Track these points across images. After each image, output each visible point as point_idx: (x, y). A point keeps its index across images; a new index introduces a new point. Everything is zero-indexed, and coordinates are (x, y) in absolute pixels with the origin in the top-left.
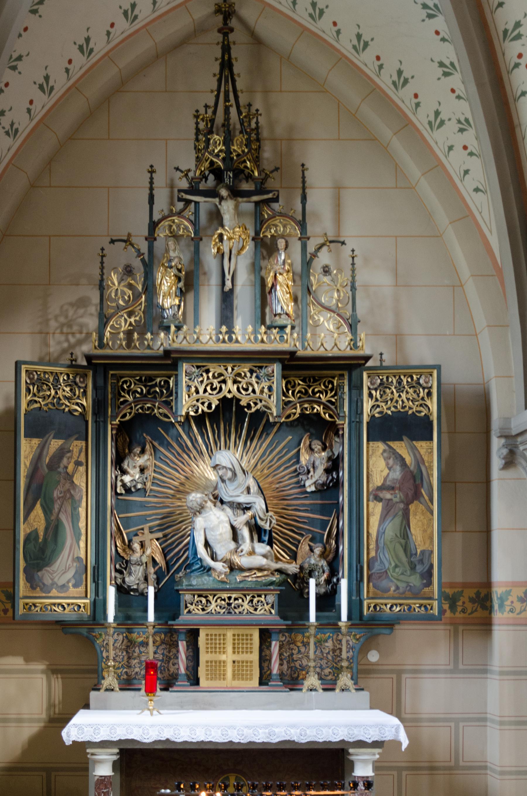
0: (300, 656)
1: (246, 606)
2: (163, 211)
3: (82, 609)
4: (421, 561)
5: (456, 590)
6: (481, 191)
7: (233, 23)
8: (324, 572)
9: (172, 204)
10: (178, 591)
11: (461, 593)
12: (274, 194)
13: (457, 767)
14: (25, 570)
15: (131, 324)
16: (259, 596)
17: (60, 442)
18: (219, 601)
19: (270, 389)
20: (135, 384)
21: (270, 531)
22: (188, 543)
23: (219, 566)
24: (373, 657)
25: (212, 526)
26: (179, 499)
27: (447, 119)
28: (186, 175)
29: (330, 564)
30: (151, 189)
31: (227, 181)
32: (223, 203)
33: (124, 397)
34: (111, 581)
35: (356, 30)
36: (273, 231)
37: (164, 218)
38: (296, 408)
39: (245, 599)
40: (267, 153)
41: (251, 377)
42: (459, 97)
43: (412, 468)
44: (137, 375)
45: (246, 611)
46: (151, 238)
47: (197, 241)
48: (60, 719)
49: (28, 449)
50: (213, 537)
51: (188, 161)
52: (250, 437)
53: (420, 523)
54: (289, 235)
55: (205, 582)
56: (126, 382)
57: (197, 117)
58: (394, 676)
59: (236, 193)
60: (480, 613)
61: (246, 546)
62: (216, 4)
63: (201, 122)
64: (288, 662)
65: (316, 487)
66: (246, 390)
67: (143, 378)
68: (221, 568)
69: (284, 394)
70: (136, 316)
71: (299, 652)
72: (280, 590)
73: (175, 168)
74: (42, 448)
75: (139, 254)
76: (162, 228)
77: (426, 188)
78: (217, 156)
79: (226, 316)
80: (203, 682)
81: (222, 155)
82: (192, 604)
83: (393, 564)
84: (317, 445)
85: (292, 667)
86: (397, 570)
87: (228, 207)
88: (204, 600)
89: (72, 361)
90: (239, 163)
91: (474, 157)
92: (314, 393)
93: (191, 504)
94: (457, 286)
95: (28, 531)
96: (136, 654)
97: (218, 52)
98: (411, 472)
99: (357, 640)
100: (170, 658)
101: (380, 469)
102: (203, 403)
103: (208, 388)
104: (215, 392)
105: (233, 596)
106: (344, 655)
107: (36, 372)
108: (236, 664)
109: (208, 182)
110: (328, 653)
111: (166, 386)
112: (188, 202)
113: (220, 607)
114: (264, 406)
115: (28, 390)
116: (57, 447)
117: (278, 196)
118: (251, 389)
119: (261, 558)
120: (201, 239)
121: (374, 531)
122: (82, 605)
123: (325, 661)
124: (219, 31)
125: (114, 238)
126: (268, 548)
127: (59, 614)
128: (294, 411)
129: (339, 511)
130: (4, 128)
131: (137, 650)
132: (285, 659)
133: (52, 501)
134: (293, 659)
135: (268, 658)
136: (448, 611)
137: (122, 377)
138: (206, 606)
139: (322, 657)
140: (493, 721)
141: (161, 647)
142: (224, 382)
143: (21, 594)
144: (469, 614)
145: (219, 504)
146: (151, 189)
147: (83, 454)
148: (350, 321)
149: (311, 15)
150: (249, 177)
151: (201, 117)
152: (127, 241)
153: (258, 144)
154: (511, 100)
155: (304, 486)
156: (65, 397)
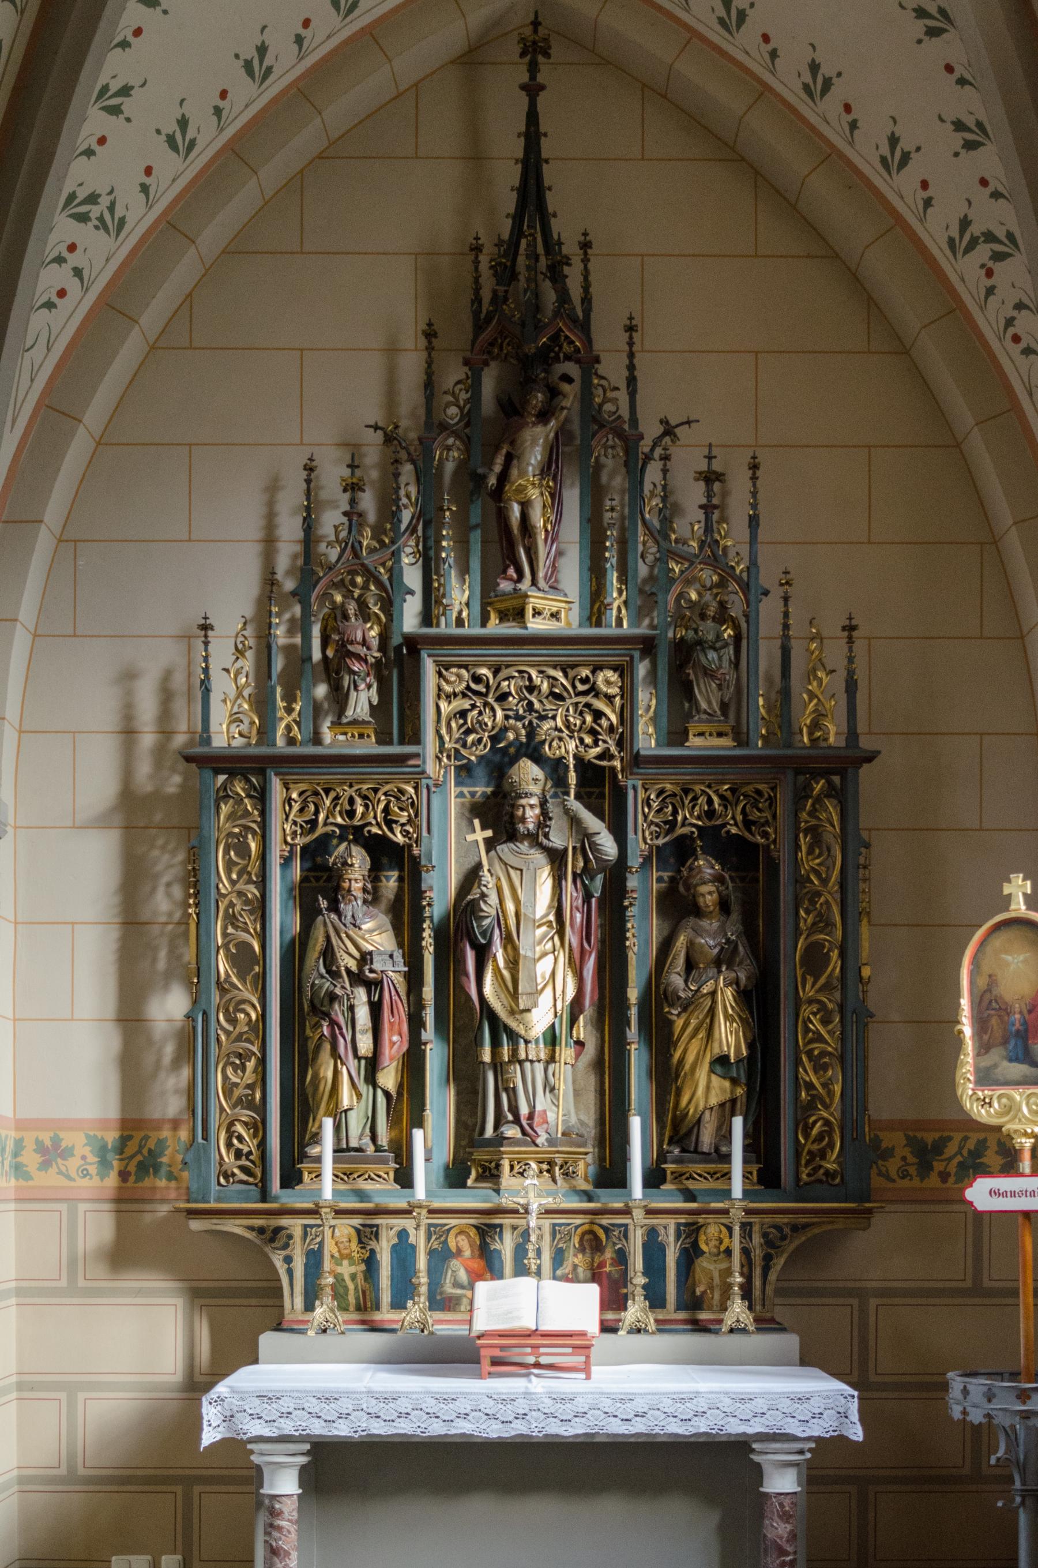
35: (808, 55)
48: (197, 1384)
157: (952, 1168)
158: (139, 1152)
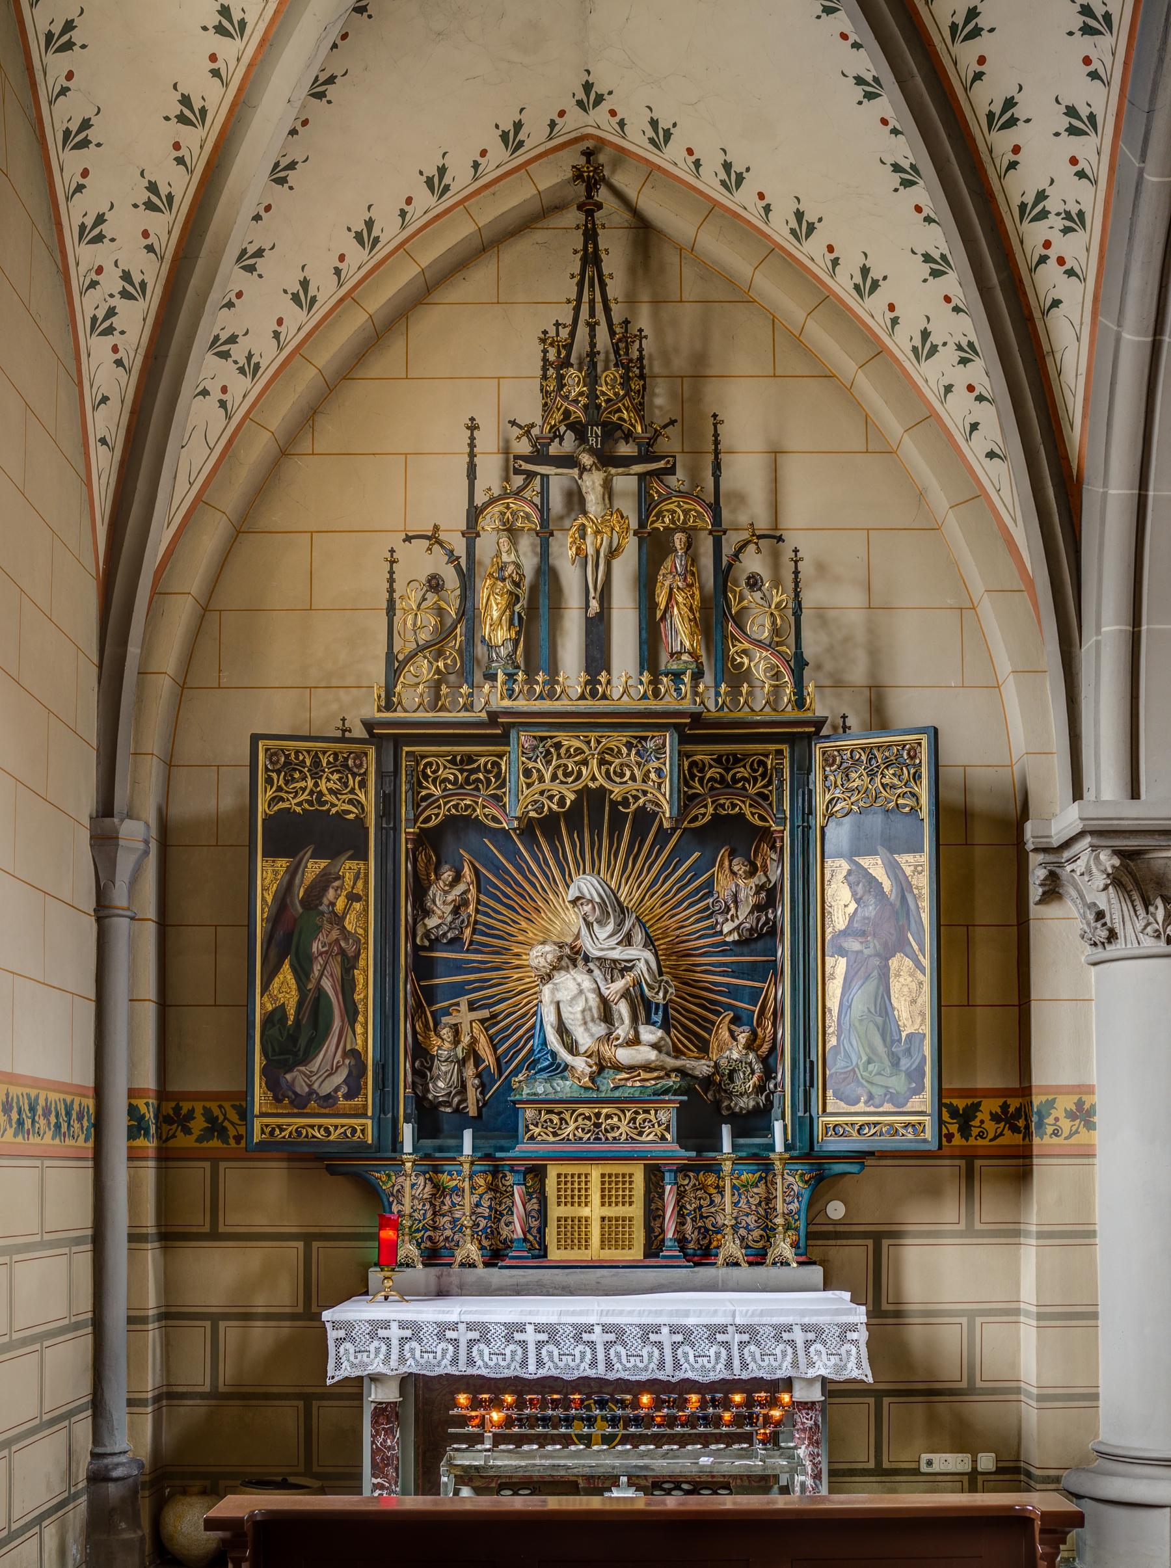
0: (713, 1210)
1: (624, 1128)
2: (490, 489)
3: (359, 1133)
4: (908, 1052)
5: (969, 1101)
6: (999, 456)
7: (602, 194)
8: (753, 1072)
9: (507, 479)
10: (514, 1102)
11: (976, 1107)
12: (668, 462)
13: (971, 1390)
14: (264, 1072)
15: (438, 671)
16: (647, 1112)
17: (323, 863)
18: (580, 1119)
19: (659, 771)
20: (445, 767)
21: (666, 1006)
22: (533, 1027)
23: (580, 1064)
24: (836, 1210)
25: (569, 997)
26: (518, 955)
27: (940, 344)
28: (527, 433)
29: (764, 1060)
30: (472, 455)
31: (592, 441)
32: (585, 476)
33: (427, 788)
34: (405, 1088)
36: (667, 520)
37: (492, 501)
38: (705, 806)
39: (622, 1117)
40: (661, 400)
41: (629, 755)
42: (957, 309)
43: (893, 898)
44: (448, 753)
45: (624, 1137)
46: (471, 533)
47: (545, 535)
49: (270, 876)
50: (572, 1016)
51: (530, 411)
52: (633, 853)
53: (905, 989)
54: (694, 528)
55: (559, 1089)
56: (430, 764)
57: (543, 341)
58: (870, 1242)
59: (606, 460)
60: (1010, 1139)
61: (623, 1030)
62: (573, 167)
63: (550, 349)
64: (694, 1220)
65: (739, 935)
66: (622, 775)
67: (459, 758)
68: (583, 1065)
69: (687, 784)
70: (445, 659)
71: (712, 1202)
72: (681, 1102)
73: (510, 422)
74: (293, 872)
75: (452, 558)
76: (488, 517)
77: (912, 451)
78: (576, 401)
79: (597, 657)
80: (555, 1254)
81: (583, 400)
82: (536, 1125)
83: (865, 1059)
84: (739, 866)
85: (700, 1228)
86: (871, 1067)
87: (594, 483)
88: (556, 1119)
89: (344, 731)
90: (610, 413)
91: (985, 403)
92: (735, 781)
93: (536, 961)
94: (966, 609)
95: (270, 1007)
96: (446, 1208)
97: (578, 240)
98: (891, 904)
99: (806, 1182)
100: (502, 1215)
101: (842, 903)
102: (551, 798)
103: (560, 773)
104: (570, 780)
105: (604, 1111)
106: (780, 1206)
107: (282, 750)
108: (606, 1222)
109: (565, 443)
110: (759, 1204)
111: (495, 770)
112: (530, 475)
113: (583, 1130)
114: (650, 801)
115: (269, 781)
116: (318, 871)
117: (674, 465)
118: (628, 773)
119: (648, 1049)
120: (552, 534)
121: (833, 1003)
122: (358, 1128)
123: (755, 1218)
124: (580, 208)
125: (410, 534)
126: (660, 1033)
127: (321, 1143)
128: (703, 810)
129: (778, 974)
130: (236, 362)
131: (447, 1200)
132: (688, 1214)
133: (310, 959)
134: (701, 1215)
135: (660, 1212)
136: (957, 1136)
137: (423, 757)
138: (560, 1129)
139: (748, 1210)
140: (1027, 1314)
141: (487, 1197)
142: (585, 762)
143: (256, 1111)
144: (991, 1140)
145: (580, 963)
146: (472, 455)
147: (360, 884)
148: (792, 663)
149: (723, 183)
150: (628, 436)
151: (549, 341)
152: (433, 538)
153: (642, 383)
154: (1037, 315)
155: (721, 932)
156: (331, 791)
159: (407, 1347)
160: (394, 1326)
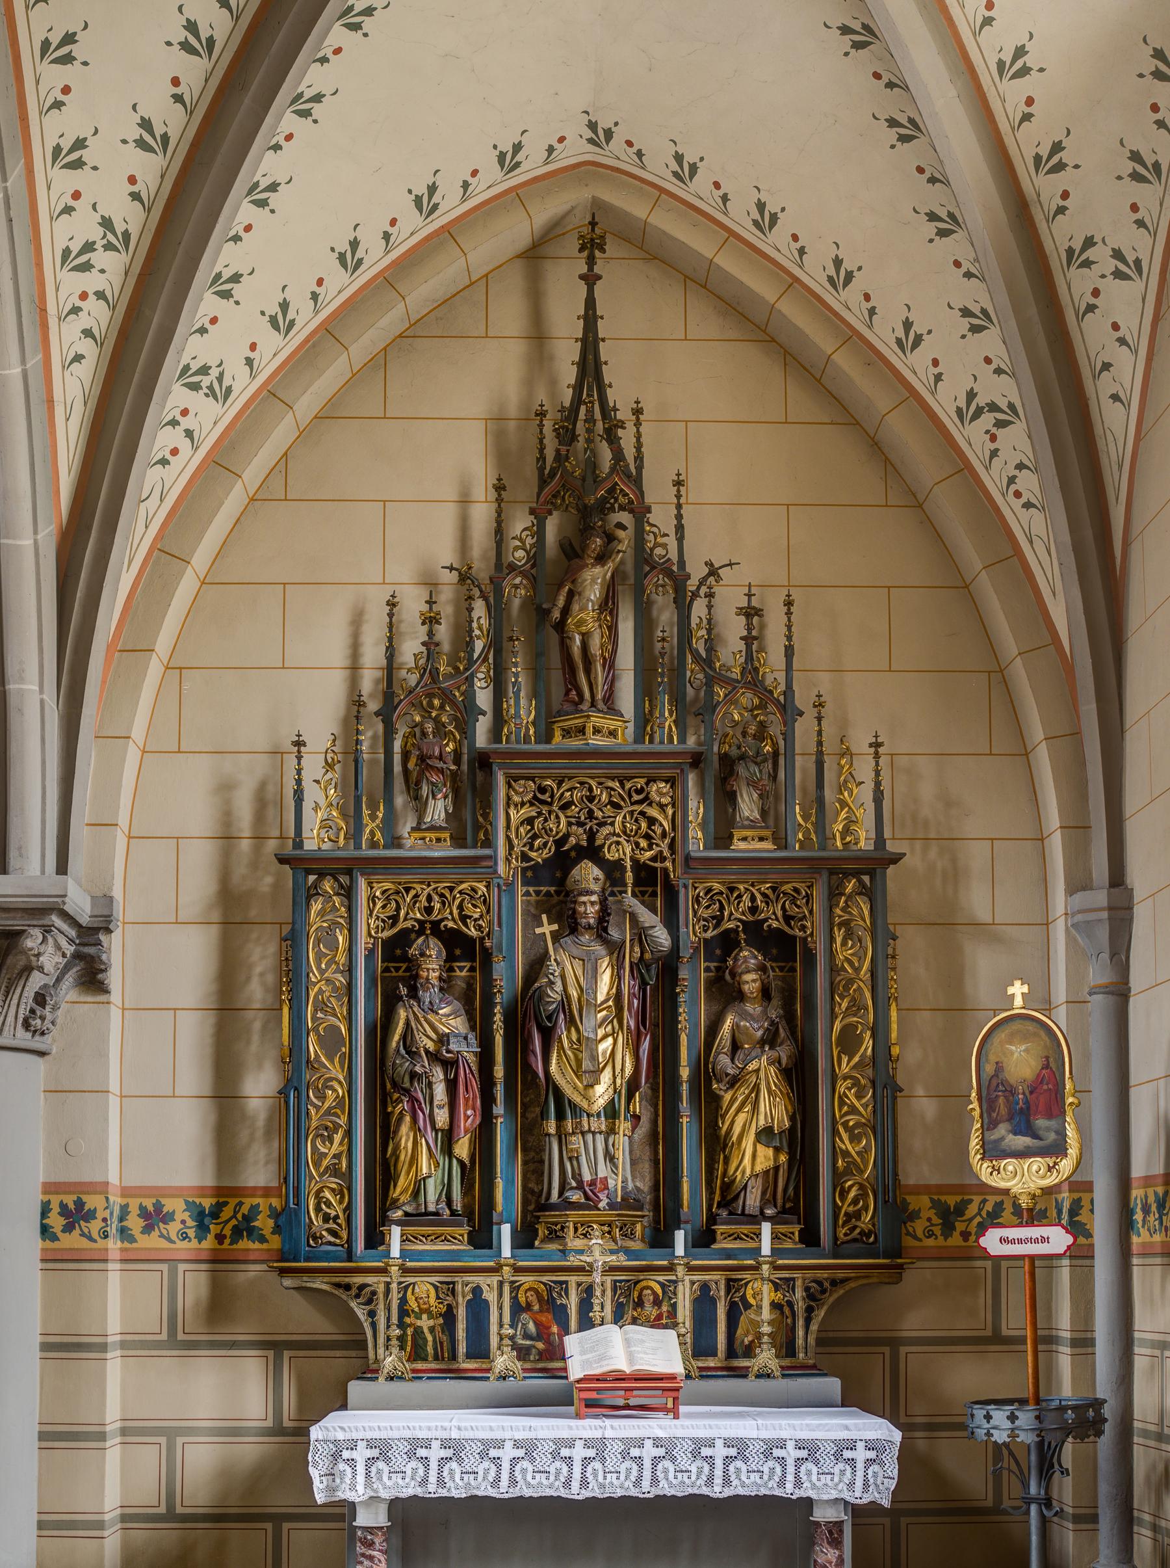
157: (227, 1231)
158: (234, 1216)
159: (660, 1467)
160: (719, 1443)
